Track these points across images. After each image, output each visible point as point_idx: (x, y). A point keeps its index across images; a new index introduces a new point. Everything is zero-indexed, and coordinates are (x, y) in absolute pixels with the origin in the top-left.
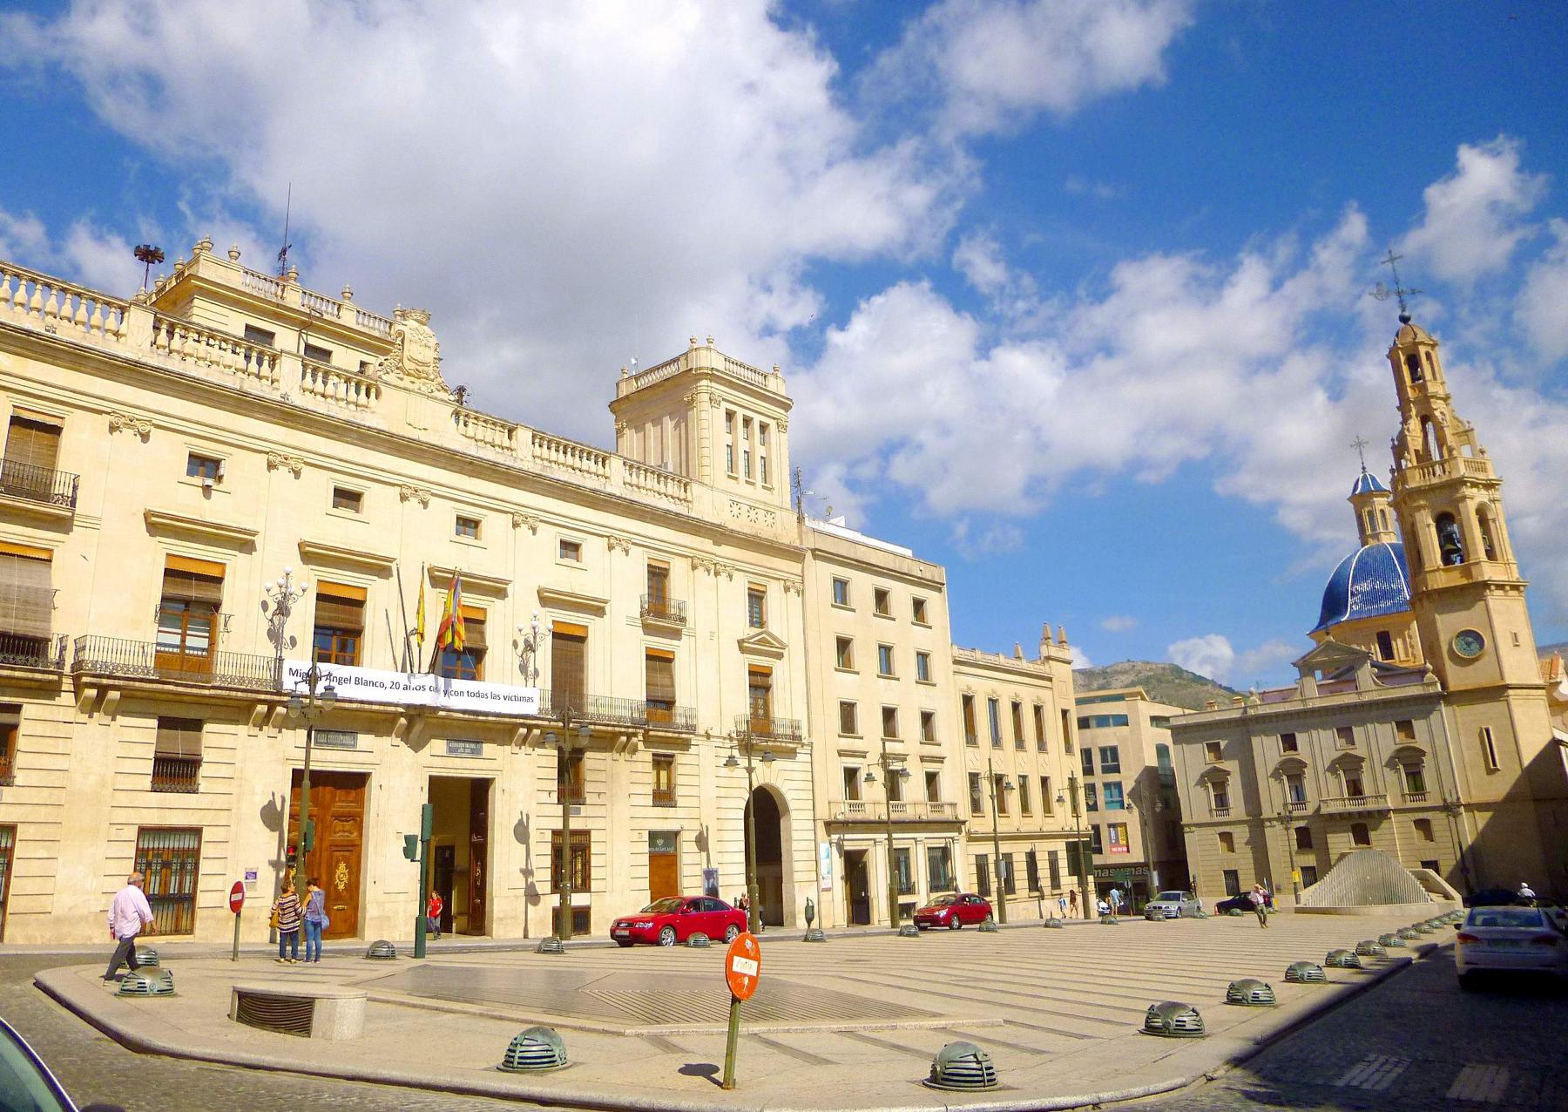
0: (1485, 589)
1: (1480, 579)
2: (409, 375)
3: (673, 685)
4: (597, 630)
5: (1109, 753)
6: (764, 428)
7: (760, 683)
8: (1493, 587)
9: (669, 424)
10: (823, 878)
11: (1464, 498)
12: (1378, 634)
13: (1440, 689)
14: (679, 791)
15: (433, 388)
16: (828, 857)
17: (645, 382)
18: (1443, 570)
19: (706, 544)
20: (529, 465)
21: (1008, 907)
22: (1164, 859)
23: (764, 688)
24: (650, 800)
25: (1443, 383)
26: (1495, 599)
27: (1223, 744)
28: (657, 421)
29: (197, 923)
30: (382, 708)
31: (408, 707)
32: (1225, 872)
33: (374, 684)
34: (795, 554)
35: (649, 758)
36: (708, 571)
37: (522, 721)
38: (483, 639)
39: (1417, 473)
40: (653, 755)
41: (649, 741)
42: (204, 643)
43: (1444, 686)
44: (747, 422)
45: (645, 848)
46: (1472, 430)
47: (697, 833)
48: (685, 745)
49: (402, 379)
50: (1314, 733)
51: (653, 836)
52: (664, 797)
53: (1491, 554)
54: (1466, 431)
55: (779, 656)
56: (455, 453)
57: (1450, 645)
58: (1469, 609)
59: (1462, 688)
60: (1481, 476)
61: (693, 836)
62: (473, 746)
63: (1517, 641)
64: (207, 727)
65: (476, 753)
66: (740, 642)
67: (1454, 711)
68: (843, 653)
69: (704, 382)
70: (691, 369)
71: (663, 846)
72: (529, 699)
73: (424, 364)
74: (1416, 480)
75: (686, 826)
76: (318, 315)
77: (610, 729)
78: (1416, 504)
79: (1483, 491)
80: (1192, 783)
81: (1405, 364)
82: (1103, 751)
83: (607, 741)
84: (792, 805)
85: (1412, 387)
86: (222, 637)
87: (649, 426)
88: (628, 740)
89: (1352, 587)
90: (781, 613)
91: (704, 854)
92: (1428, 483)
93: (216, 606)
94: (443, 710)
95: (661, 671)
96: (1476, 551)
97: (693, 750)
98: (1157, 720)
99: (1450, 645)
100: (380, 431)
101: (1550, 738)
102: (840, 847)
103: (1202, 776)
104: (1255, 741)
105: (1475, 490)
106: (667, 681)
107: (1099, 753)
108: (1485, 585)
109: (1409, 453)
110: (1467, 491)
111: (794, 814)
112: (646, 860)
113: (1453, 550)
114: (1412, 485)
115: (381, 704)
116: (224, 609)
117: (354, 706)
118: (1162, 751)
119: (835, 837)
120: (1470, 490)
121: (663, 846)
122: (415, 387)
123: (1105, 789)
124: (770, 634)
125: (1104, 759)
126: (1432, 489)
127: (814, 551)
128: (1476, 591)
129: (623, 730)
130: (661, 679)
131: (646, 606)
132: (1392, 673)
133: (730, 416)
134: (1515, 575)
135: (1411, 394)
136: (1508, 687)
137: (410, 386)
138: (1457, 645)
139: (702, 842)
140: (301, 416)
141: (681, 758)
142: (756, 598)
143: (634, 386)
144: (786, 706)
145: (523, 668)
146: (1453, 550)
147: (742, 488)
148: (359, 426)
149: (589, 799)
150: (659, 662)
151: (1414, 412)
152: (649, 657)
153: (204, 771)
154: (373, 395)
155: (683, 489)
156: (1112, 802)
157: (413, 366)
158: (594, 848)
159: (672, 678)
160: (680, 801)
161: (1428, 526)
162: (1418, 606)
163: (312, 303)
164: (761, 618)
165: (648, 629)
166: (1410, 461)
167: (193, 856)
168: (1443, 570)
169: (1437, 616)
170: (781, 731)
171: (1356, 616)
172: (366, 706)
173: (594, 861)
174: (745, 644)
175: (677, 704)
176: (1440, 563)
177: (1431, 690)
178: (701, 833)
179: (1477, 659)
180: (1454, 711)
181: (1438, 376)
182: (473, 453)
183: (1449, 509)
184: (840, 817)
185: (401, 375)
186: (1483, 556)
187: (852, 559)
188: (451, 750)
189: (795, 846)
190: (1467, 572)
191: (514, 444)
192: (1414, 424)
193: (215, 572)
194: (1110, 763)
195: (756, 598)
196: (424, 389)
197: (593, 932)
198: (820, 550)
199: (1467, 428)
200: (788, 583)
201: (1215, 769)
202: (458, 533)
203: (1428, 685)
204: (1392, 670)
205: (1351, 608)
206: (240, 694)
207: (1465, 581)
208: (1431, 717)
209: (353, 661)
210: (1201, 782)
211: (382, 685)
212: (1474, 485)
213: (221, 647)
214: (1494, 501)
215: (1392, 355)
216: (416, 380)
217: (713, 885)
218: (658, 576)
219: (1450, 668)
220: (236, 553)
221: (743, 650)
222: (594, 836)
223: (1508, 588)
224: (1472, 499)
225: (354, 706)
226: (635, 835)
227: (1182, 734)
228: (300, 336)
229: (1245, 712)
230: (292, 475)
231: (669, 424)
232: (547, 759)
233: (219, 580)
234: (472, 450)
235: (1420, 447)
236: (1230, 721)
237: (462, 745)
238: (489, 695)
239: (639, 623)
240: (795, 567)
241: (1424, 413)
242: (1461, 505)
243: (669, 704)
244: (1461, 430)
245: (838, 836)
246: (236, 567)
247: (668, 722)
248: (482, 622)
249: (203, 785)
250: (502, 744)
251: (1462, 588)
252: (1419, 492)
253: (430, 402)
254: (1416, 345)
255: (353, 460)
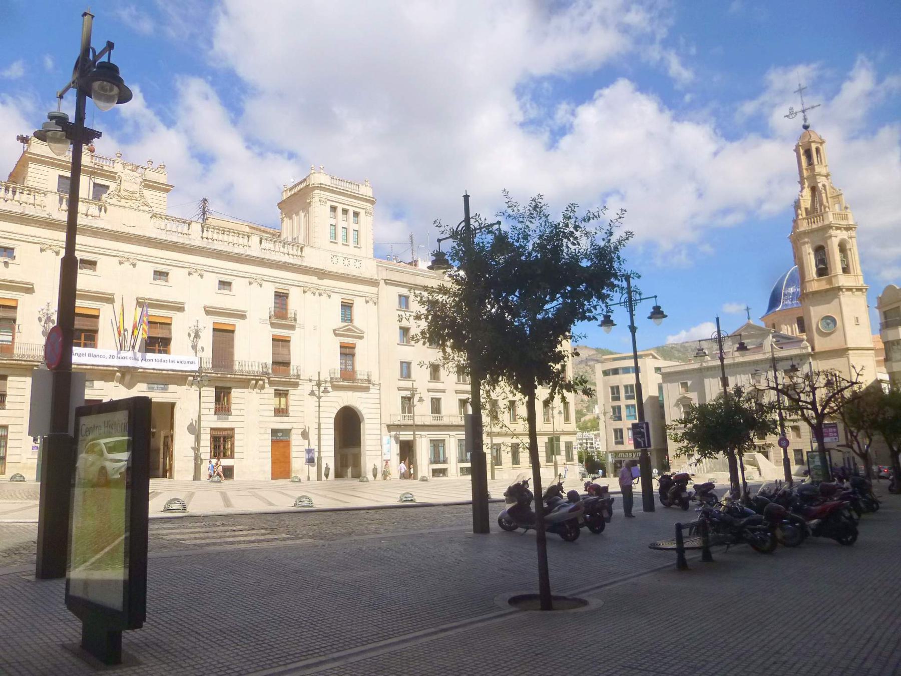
0: (839, 292)
1: (837, 285)
2: (125, 199)
3: (290, 354)
4: (240, 327)
5: (629, 388)
6: (356, 214)
7: (347, 352)
8: (844, 290)
9: (302, 214)
10: (385, 454)
11: (831, 236)
12: (797, 318)
13: (810, 350)
14: (291, 408)
15: (139, 205)
16: (388, 443)
17: (293, 192)
18: (816, 280)
19: (314, 279)
20: (198, 243)
21: (496, 472)
22: (659, 447)
23: (351, 355)
24: (272, 413)
25: (826, 166)
26: (845, 298)
27: (689, 383)
28: (297, 214)
29: (7, 470)
30: (105, 368)
31: (120, 367)
32: (794, 450)
33: (100, 356)
34: (374, 283)
35: (272, 391)
36: (314, 294)
37: (189, 374)
38: (170, 332)
39: (805, 222)
40: (275, 390)
41: (271, 383)
42: (10, 338)
43: (813, 349)
44: (345, 212)
45: (269, 437)
46: (841, 194)
47: (302, 430)
48: (296, 385)
49: (120, 201)
50: (738, 376)
51: (274, 432)
52: (281, 412)
53: (846, 270)
54: (838, 195)
55: (361, 338)
56: (150, 238)
57: (818, 325)
58: (829, 303)
59: (823, 350)
60: (844, 223)
61: (300, 431)
62: (163, 386)
63: (857, 322)
64: (9, 378)
65: (165, 390)
66: (334, 330)
67: (817, 364)
68: (406, 335)
69: (316, 191)
70: (309, 185)
71: (282, 436)
72: (192, 363)
73: (133, 192)
74: (804, 226)
75: (295, 425)
76: (100, 168)
77: (244, 377)
78: (803, 241)
79: (844, 232)
80: (672, 405)
81: (803, 155)
82: (626, 387)
83: (245, 383)
84: (365, 417)
85: (807, 170)
86: (17, 335)
87: (294, 216)
88: (257, 383)
89: (785, 290)
90: (362, 315)
91: (306, 441)
92: (810, 228)
93: (15, 321)
94: (141, 368)
95: (283, 346)
96: (835, 269)
97: (300, 387)
98: (658, 369)
99: (818, 325)
100: (103, 229)
101: (875, 379)
102: (396, 438)
103: (678, 401)
104: (706, 381)
105: (839, 231)
106: (286, 352)
107: (623, 388)
108: (839, 289)
109: (801, 210)
110: (833, 232)
111: (366, 421)
112: (269, 443)
113: (823, 271)
114: (801, 229)
115: (104, 366)
116: (17, 322)
117: (100, 368)
118: (660, 388)
119: (393, 433)
120: (835, 231)
121: (282, 436)
122: (128, 205)
123: (627, 408)
124: (353, 326)
125: (626, 392)
126: (812, 231)
127: (385, 280)
128: (834, 292)
129: (252, 377)
130: (283, 351)
131: (273, 313)
132: (791, 341)
133: (334, 209)
134: (861, 282)
135: (805, 174)
136: (848, 349)
137: (125, 205)
138: (821, 324)
139: (305, 435)
140: (58, 224)
141: (292, 391)
142: (347, 307)
143: (289, 194)
144: (363, 365)
145: (194, 347)
146: (823, 271)
147: (339, 248)
148: (91, 227)
149: (234, 412)
150: (280, 343)
151: (806, 184)
152: (274, 340)
153: (8, 399)
154: (103, 210)
155: (300, 250)
156: (630, 416)
157: (127, 194)
158: (236, 437)
159: (289, 350)
160: (291, 414)
161: (809, 254)
162: (803, 302)
163: (97, 161)
164: (351, 318)
165: (273, 325)
166: (802, 213)
167: (4, 439)
168: (816, 280)
169: (811, 308)
170: (359, 377)
171: (785, 308)
172: (96, 367)
173: (236, 443)
174: (337, 332)
175: (291, 364)
176: (815, 276)
177: (804, 351)
178: (305, 430)
179: (830, 334)
180: (817, 364)
181: (823, 161)
182: (163, 238)
183: (822, 244)
184: (396, 423)
185: (119, 199)
186: (840, 271)
187: (412, 284)
188: (149, 388)
189: (367, 437)
190: (830, 282)
191: (190, 232)
192: (807, 193)
193: (12, 304)
194: (630, 394)
195: (347, 307)
196: (132, 205)
197: (175, 478)
198: (388, 280)
199: (839, 194)
200: (367, 299)
201: (685, 397)
202: (154, 279)
203: (803, 348)
204: (792, 339)
205: (783, 303)
206: (23, 363)
207: (828, 287)
208: (804, 366)
209: (94, 346)
210: (677, 405)
211: (104, 357)
212: (837, 228)
213: (16, 340)
214: (851, 238)
215: (797, 151)
216: (129, 201)
217: (311, 456)
218: (281, 297)
219: (817, 339)
220: (24, 294)
221: (336, 335)
222: (236, 431)
223: (854, 290)
224: (836, 237)
225: (88, 367)
226: (262, 431)
227: (668, 377)
228: (90, 179)
229: (701, 365)
230: (54, 254)
231: (302, 214)
232: (209, 393)
233: (15, 308)
234: (163, 236)
235: (809, 206)
236: (693, 370)
237: (156, 386)
238: (168, 361)
239: (268, 322)
240: (374, 290)
241: (812, 185)
242: (829, 242)
243: (287, 364)
244: (835, 195)
245: (395, 433)
246: (23, 300)
247: (287, 374)
248: (170, 324)
249: (8, 405)
250: (180, 385)
251: (827, 291)
252: (805, 233)
253: (137, 212)
254: (810, 143)
255: (91, 245)
